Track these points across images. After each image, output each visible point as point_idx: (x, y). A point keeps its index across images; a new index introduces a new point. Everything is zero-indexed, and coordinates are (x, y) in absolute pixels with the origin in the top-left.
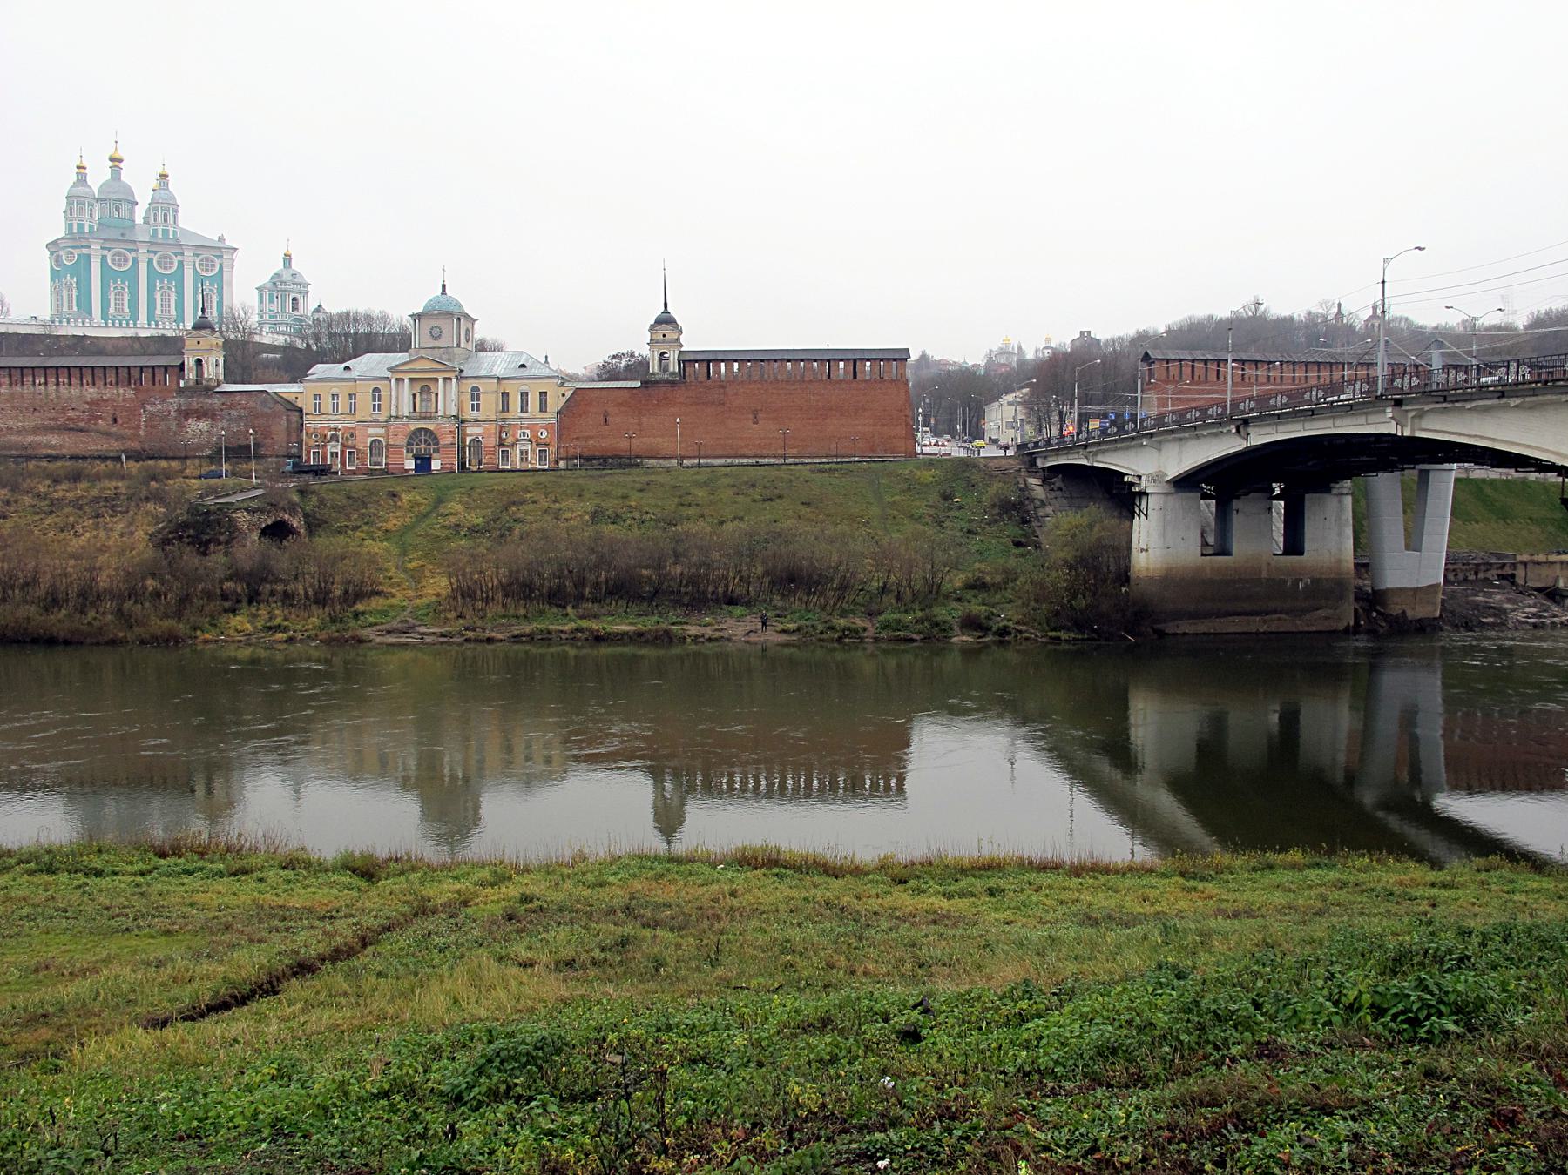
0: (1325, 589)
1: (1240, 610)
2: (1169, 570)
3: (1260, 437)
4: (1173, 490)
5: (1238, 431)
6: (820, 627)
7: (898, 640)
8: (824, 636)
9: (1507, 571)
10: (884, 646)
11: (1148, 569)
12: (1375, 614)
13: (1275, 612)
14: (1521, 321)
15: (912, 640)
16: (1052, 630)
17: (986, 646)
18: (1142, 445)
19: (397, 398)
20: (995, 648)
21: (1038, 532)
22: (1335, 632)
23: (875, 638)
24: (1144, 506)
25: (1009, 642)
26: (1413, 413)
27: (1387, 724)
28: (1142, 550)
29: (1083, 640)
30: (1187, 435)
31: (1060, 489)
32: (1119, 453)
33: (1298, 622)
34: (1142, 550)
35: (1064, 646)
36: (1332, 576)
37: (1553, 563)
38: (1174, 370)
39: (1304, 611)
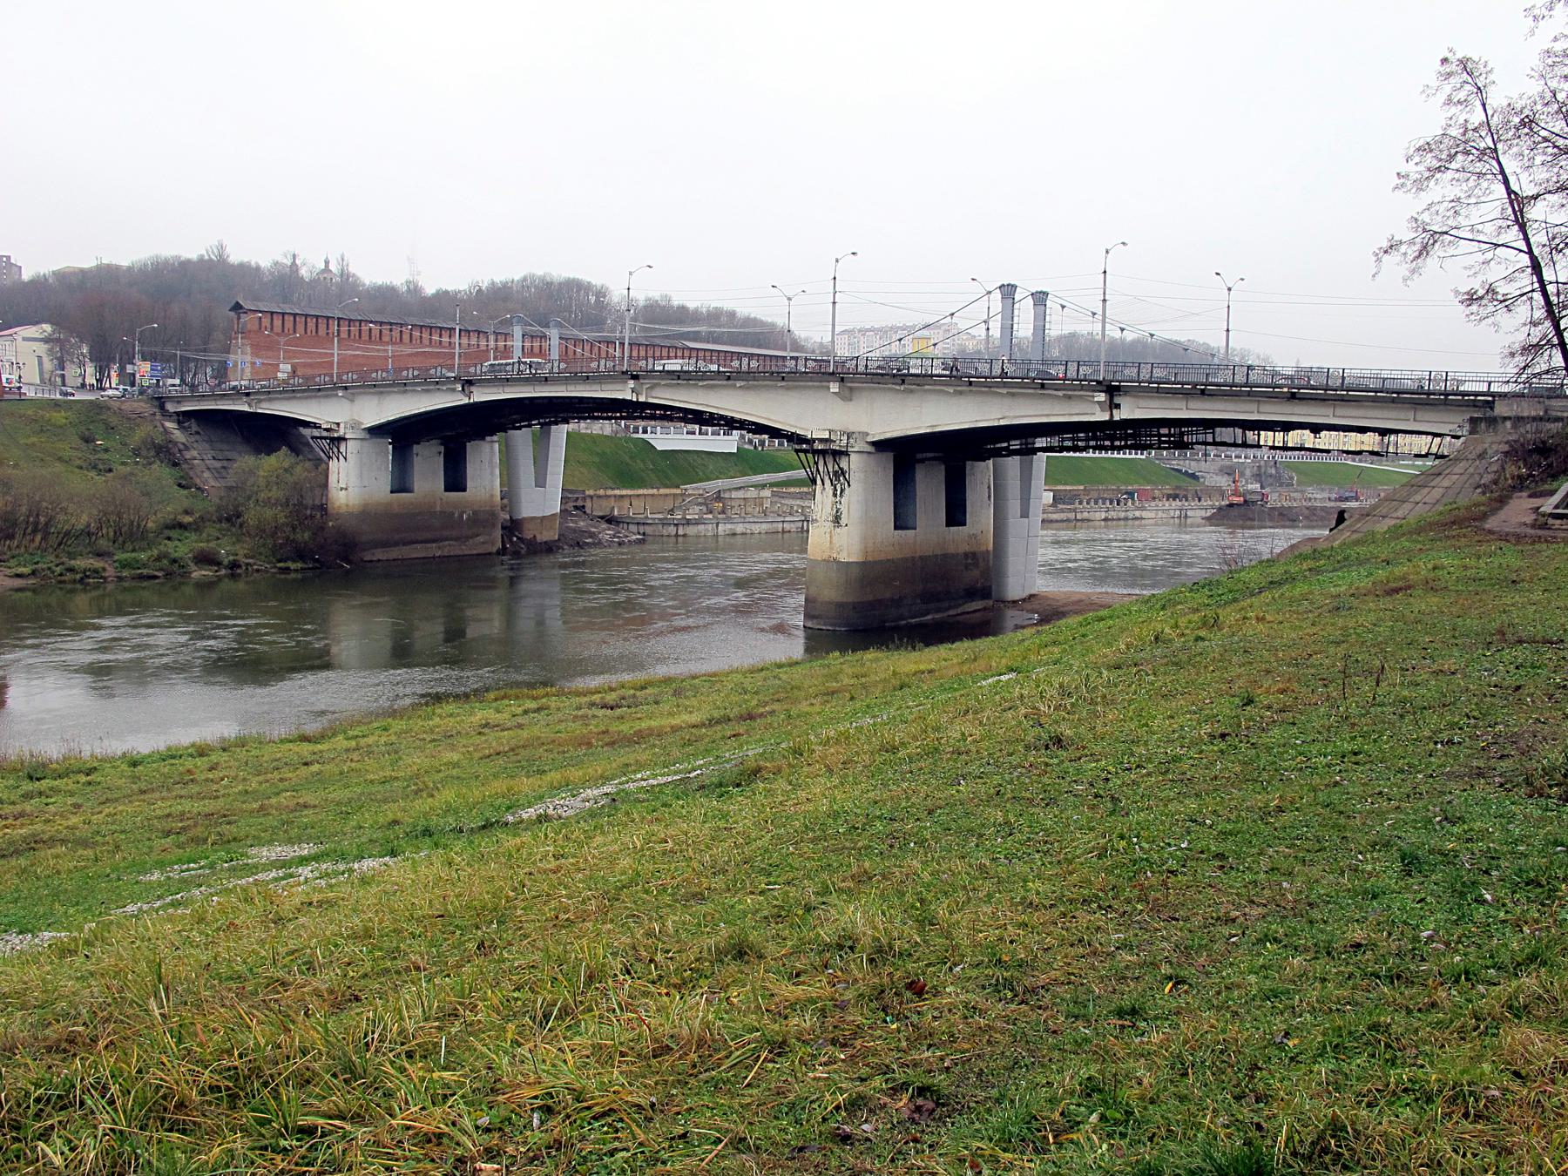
0: (481, 519)
1: (420, 539)
2: (366, 505)
3: (480, 395)
4: (368, 436)
5: (463, 389)
6: (58, 570)
7: (141, 577)
8: (63, 578)
9: (580, 503)
10: (126, 584)
11: (347, 506)
12: (515, 539)
13: (447, 539)
14: (430, 290)
15: (155, 577)
16: (280, 561)
17: (220, 579)
18: (337, 395)
19: (934, 390)
20: (226, 580)
21: (191, 474)
22: (490, 554)
23: (118, 577)
24: (342, 449)
25: (240, 575)
26: (647, 386)
27: (525, 624)
28: (342, 489)
29: (309, 569)
30: (396, 389)
31: (198, 433)
32: (286, 402)
33: (464, 547)
34: (342, 489)
35: (293, 575)
36: (487, 508)
37: (610, 496)
38: (278, 322)
39: (468, 538)
